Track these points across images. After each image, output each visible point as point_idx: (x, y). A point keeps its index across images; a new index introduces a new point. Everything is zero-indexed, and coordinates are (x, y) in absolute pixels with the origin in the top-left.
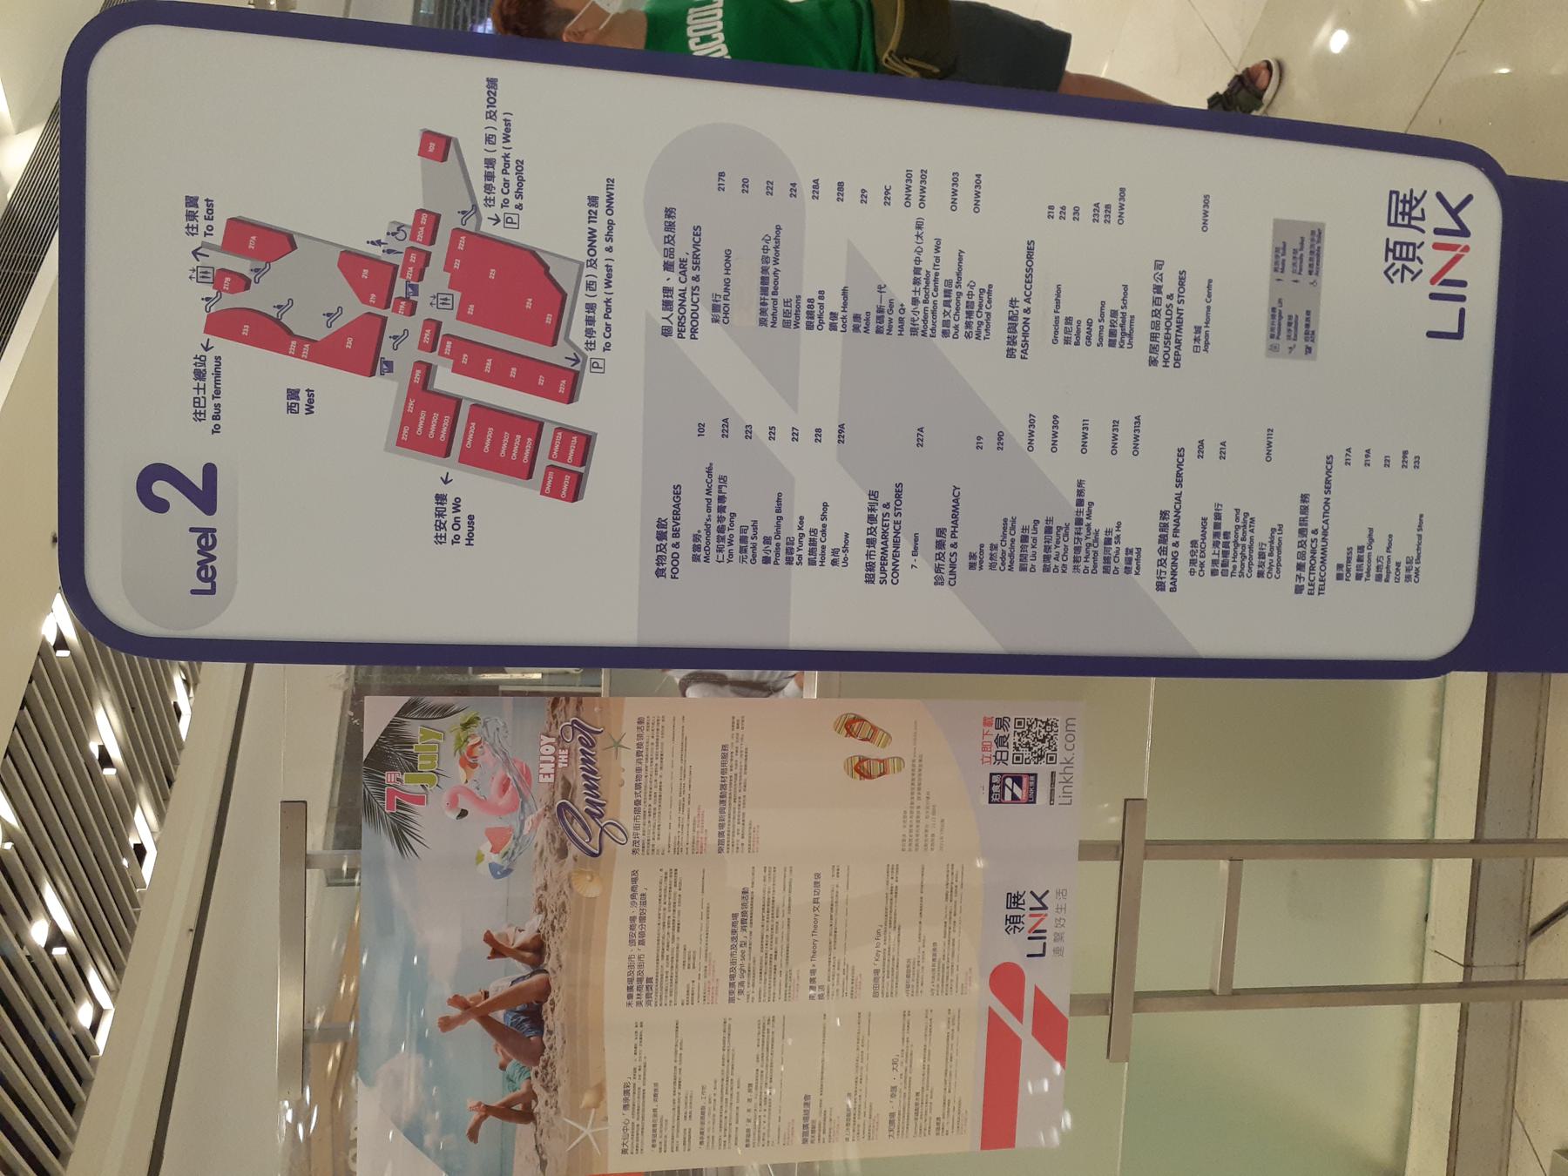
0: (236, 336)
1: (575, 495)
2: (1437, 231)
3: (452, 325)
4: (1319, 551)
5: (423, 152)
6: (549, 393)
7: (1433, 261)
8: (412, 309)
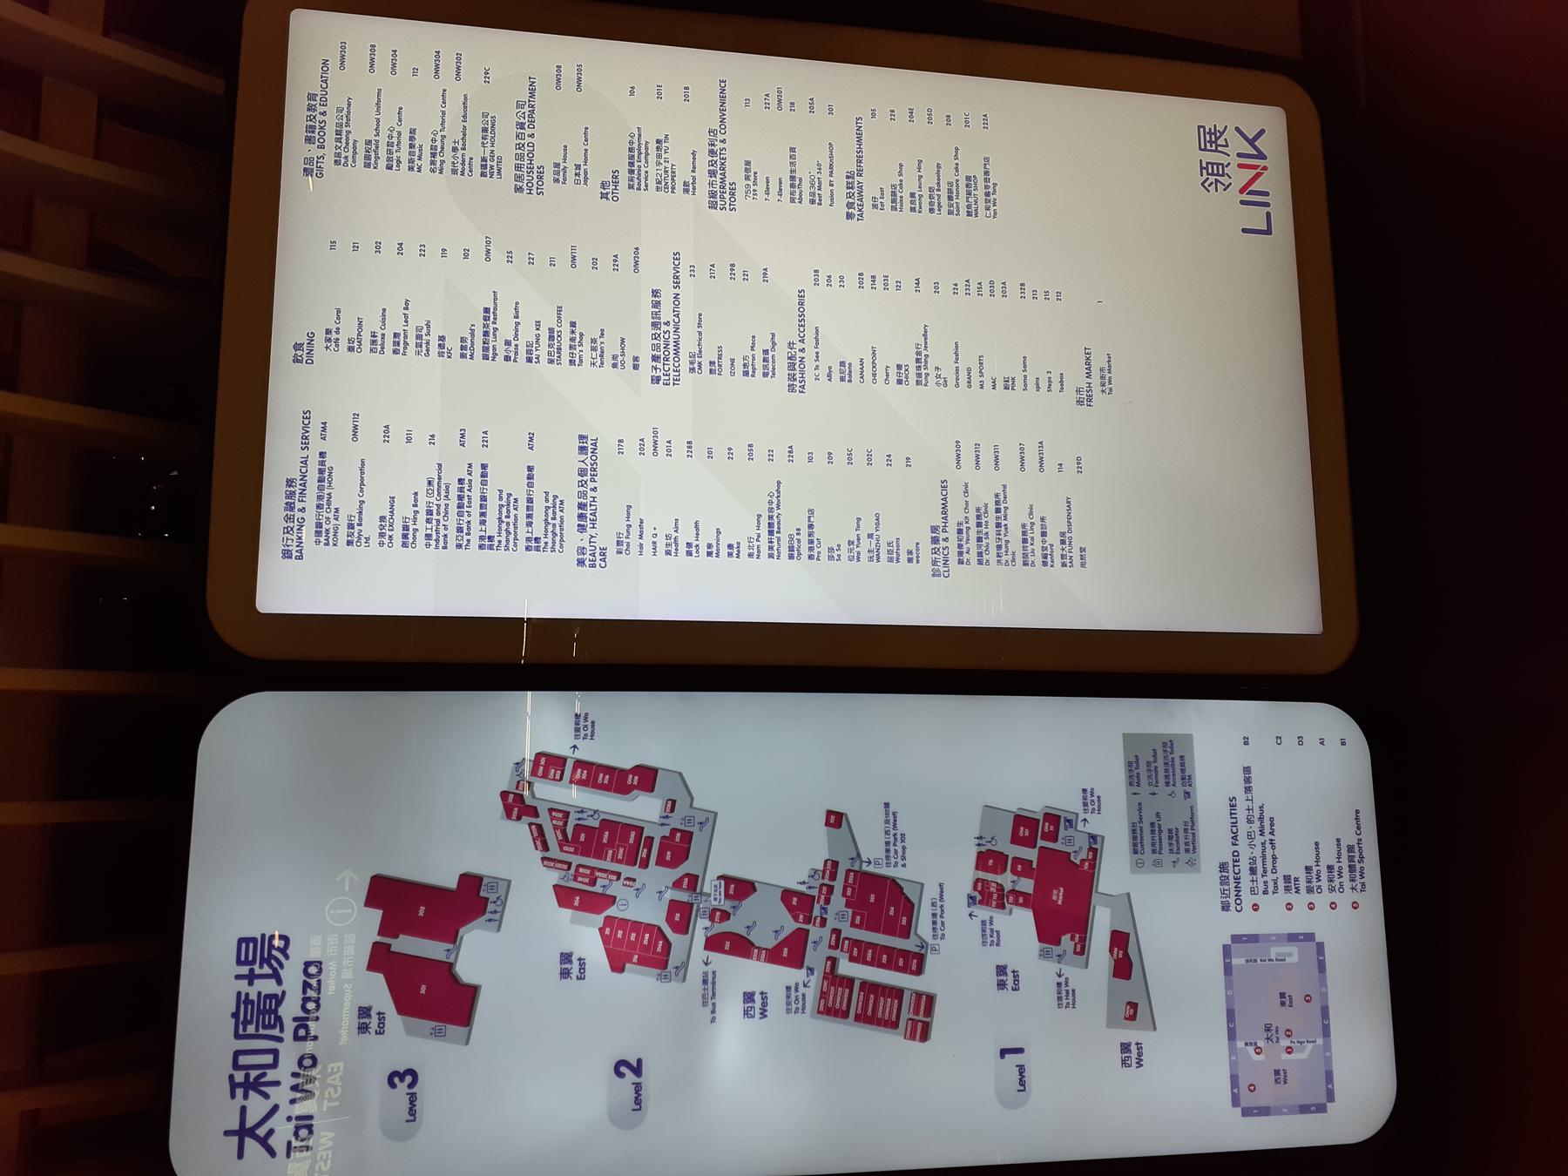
0: (721, 950)
1: (925, 1037)
2: (1239, 155)
3: (849, 932)
5: (827, 824)
6: (905, 969)
7: (1240, 177)
8: (823, 923)
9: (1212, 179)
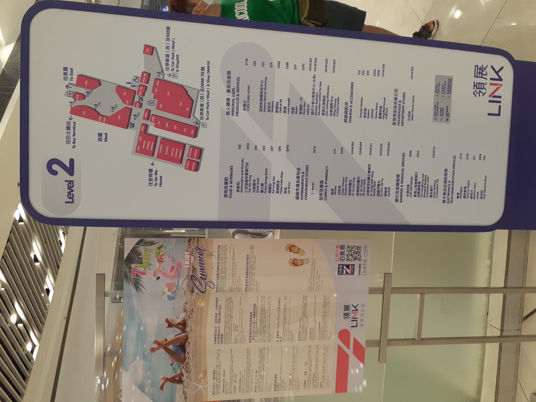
0: (81, 115)
1: (197, 169)
2: (491, 79)
3: (154, 111)
4: (451, 188)
5: (145, 52)
6: (188, 134)
7: (490, 89)
8: (141, 106)
9: (478, 90)
